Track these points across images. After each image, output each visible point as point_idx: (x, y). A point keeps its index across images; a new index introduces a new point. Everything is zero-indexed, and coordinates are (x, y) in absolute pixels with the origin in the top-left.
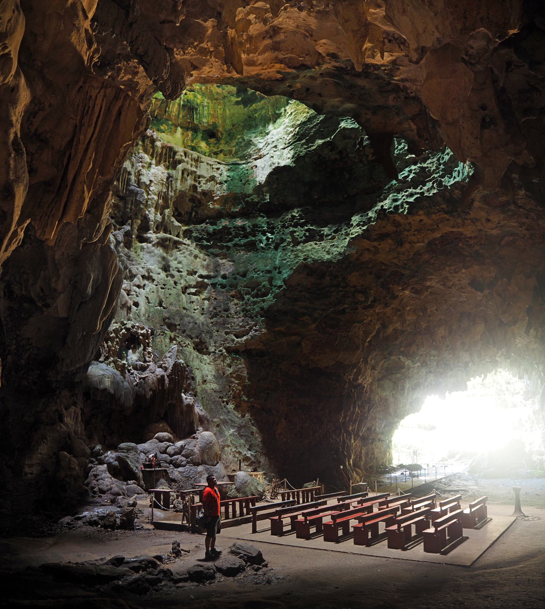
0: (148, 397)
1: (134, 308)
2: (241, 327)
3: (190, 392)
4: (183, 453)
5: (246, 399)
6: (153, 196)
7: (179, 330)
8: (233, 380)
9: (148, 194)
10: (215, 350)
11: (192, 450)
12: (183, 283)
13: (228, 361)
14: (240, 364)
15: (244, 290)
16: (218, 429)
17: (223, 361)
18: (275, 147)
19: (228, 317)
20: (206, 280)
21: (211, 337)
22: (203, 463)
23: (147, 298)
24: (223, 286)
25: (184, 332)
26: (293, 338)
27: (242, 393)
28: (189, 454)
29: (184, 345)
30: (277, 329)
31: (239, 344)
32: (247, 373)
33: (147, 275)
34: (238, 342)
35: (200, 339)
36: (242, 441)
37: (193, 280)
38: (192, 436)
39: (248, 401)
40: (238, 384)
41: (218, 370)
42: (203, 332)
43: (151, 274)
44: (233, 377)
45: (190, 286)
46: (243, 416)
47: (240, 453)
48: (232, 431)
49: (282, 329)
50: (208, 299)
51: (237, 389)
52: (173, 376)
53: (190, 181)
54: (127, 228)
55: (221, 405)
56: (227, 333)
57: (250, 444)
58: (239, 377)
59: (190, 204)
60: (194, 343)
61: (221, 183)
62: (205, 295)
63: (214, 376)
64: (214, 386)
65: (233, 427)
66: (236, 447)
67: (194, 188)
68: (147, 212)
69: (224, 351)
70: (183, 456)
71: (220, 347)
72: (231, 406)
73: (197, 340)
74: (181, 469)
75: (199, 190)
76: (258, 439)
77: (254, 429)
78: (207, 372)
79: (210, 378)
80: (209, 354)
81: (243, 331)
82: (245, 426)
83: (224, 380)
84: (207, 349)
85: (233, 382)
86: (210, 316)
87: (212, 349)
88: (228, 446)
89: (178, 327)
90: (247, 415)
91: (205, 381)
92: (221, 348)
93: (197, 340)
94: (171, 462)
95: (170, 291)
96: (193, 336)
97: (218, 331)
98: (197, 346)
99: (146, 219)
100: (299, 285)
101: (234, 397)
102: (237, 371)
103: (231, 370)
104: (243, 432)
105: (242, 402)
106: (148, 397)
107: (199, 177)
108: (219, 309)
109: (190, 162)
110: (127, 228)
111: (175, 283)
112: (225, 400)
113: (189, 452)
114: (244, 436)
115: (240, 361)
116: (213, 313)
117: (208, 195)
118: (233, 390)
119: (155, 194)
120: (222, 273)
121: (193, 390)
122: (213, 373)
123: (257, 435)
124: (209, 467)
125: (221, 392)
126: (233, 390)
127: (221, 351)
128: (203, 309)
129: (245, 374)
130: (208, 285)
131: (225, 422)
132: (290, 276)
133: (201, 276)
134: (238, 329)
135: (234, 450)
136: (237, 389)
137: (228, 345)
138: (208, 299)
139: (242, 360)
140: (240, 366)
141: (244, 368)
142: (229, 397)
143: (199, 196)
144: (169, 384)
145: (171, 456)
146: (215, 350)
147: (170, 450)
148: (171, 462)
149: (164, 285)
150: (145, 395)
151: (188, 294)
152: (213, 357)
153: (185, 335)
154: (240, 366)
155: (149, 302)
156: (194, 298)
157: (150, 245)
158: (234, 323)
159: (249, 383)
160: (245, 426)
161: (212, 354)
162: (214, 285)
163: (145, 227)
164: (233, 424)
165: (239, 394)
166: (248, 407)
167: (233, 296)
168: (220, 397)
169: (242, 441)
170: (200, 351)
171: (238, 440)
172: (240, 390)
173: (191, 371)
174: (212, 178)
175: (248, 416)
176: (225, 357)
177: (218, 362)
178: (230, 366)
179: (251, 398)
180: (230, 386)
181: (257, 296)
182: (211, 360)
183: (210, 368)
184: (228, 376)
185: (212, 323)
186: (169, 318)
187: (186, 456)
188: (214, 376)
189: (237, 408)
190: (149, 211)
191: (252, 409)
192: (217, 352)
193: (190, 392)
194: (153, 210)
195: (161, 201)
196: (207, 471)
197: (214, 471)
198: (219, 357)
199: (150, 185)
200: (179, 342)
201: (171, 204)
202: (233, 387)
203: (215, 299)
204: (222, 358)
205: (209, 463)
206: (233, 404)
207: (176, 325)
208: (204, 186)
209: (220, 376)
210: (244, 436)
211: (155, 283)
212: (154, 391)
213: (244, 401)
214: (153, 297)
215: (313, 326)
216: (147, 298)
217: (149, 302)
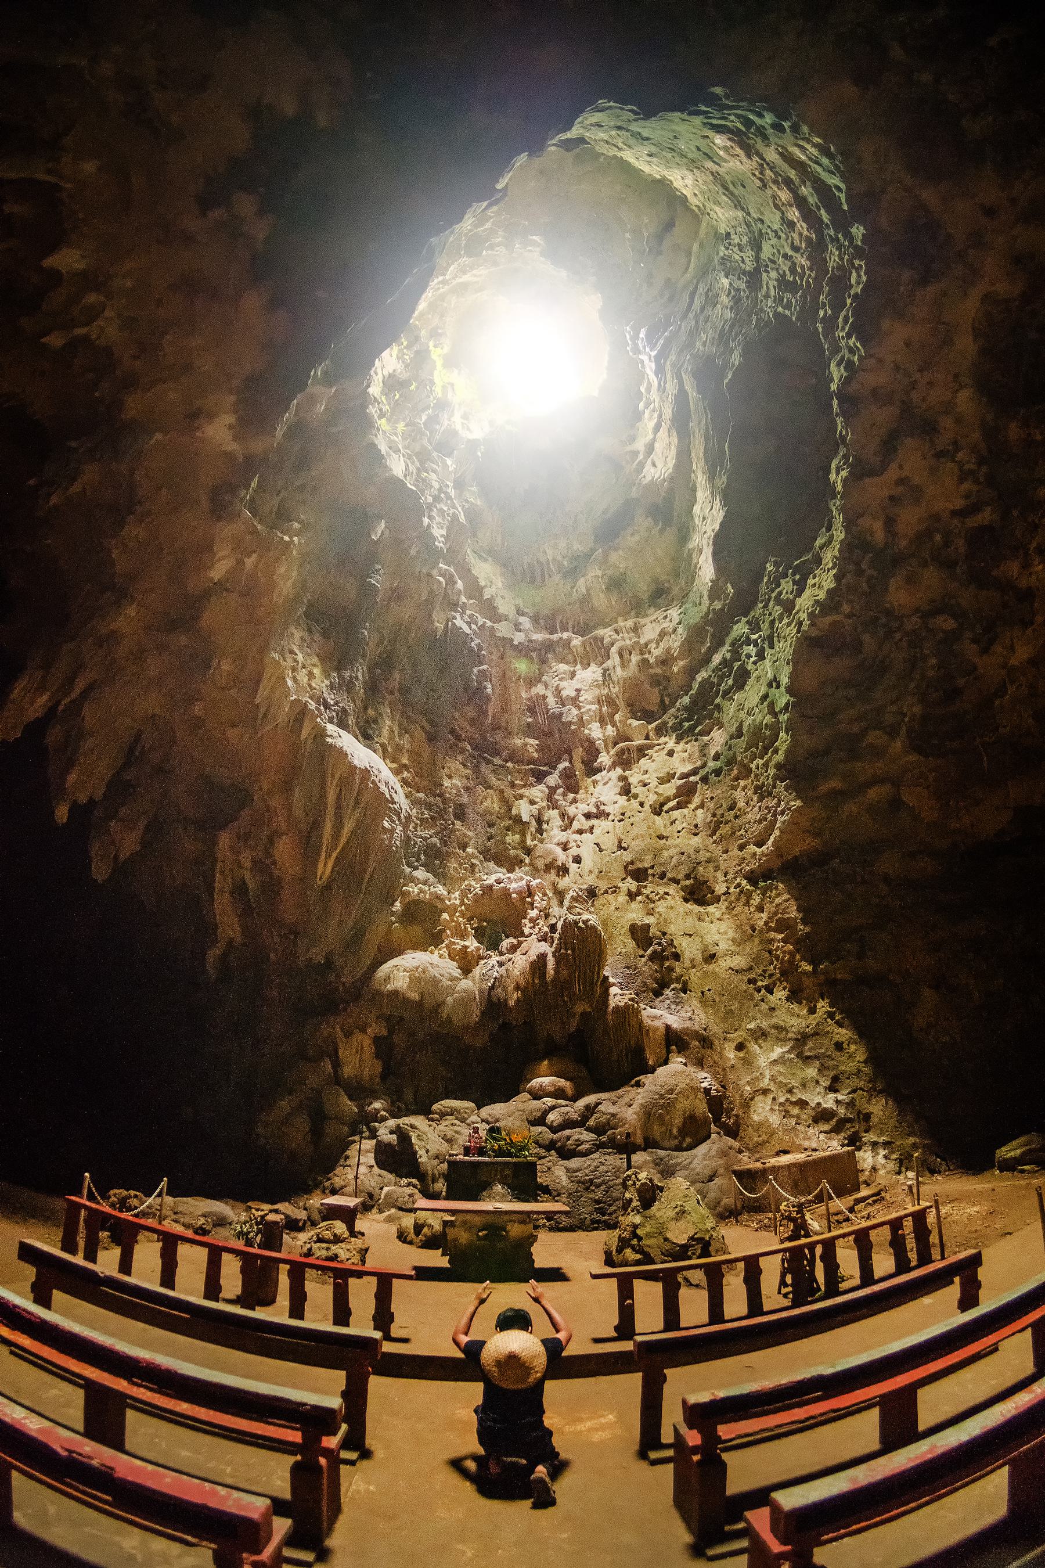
0: (511, 1003)
1: (573, 867)
2: (760, 821)
3: (672, 986)
4: (591, 1122)
5: (809, 968)
6: (588, 707)
7: (654, 875)
8: (772, 935)
9: (580, 708)
10: (728, 888)
11: (614, 1115)
12: (652, 798)
13: (756, 900)
14: (778, 895)
15: (746, 757)
16: (741, 1054)
17: (747, 904)
18: (704, 518)
19: (736, 817)
20: (692, 779)
21: (717, 869)
22: (649, 1144)
23: (597, 844)
24: (717, 772)
25: (663, 876)
26: (873, 793)
27: (798, 957)
28: (604, 1126)
29: (657, 898)
30: (823, 788)
31: (766, 856)
32: (799, 910)
33: (594, 810)
34: (763, 854)
35: (695, 878)
36: (811, 1072)
37: (669, 789)
38: (633, 1082)
39: (815, 971)
40: (784, 940)
41: (740, 927)
42: (699, 863)
43: (602, 807)
44: (770, 929)
45: (669, 799)
46: (812, 1011)
47: (802, 1104)
48: (778, 1051)
49: (835, 783)
50: (702, 806)
51: (784, 952)
52: (563, 951)
53: (635, 659)
54: (564, 765)
55: (752, 999)
56: (741, 848)
57: (832, 1074)
58: (783, 925)
59: (656, 690)
60: (683, 889)
61: (675, 630)
62: (696, 800)
63: (734, 940)
64: (739, 961)
65: (780, 1041)
66: (790, 1091)
67: (645, 661)
68: (586, 731)
69: (744, 882)
70: (589, 1129)
71: (735, 878)
72: (780, 994)
73: (688, 882)
74: (574, 1163)
75: (652, 660)
76: (855, 1057)
77: (843, 1034)
78: (717, 937)
79: (724, 946)
80: (718, 899)
81: (766, 827)
82: (816, 1034)
83: (757, 941)
84: (713, 892)
85: (771, 941)
86: (709, 832)
87: (720, 888)
88: (765, 1092)
89: (650, 871)
90: (819, 1005)
91: (713, 956)
92: (738, 880)
93: (688, 882)
94: (550, 1146)
95: (632, 820)
96: (680, 876)
97: (726, 852)
98: (691, 893)
99: (591, 742)
100: (824, 683)
101: (784, 973)
102: (776, 913)
103: (764, 916)
104: (810, 1049)
105: (804, 978)
106: (511, 1003)
107: (646, 645)
108: (719, 812)
109: (626, 635)
110: (564, 765)
111: (642, 804)
112: (760, 983)
113: (603, 1119)
114: (817, 1057)
115: (776, 888)
116: (713, 825)
117: (665, 661)
118: (777, 959)
119: (593, 703)
120: (713, 753)
121: (678, 980)
122: (731, 934)
123: (853, 1047)
124: (661, 1153)
125: (751, 968)
126: (777, 958)
127: (739, 885)
128: (696, 826)
129: (793, 913)
130: (697, 783)
131: (760, 1035)
132: (793, 676)
133: (684, 776)
134: (757, 829)
135: (782, 1100)
136: (784, 952)
137: (748, 868)
138: (702, 806)
139: (781, 886)
140: (778, 900)
141: (787, 901)
142: (771, 976)
143: (658, 671)
144: (555, 970)
145: (554, 1130)
146: (728, 888)
147: (552, 1117)
148: (550, 1146)
149: (623, 814)
150: (505, 1000)
151: (666, 812)
152: (726, 904)
153: (665, 880)
154: (778, 900)
155: (601, 850)
156: (676, 814)
157: (604, 773)
158: (749, 823)
159: (807, 929)
160: (816, 1034)
161: (723, 898)
162: (705, 780)
163: (592, 752)
164: (782, 1036)
165: (792, 962)
166: (820, 984)
167: (737, 779)
168: (750, 981)
169: (811, 1072)
170: (701, 902)
171: (798, 1072)
172: (790, 952)
173: (671, 943)
174: (663, 634)
175: (823, 1006)
176: (749, 897)
177: (738, 909)
178: (760, 909)
179: (821, 963)
180: (770, 952)
181: (766, 750)
182: (724, 910)
183: (723, 926)
184: (761, 931)
185: (715, 842)
186: (632, 863)
187: (599, 1130)
188: (734, 940)
189: (794, 996)
190: (590, 729)
191: (830, 988)
192: (732, 890)
193: (672, 986)
194: (595, 725)
195: (605, 709)
196: (657, 1165)
197: (677, 1164)
198: (738, 899)
199: (578, 696)
200: (647, 896)
201: (621, 704)
202: (776, 950)
203: (712, 798)
204: (743, 899)
205: (666, 1144)
206: (784, 989)
207: (646, 870)
208: (657, 652)
209: (748, 933)
210: (817, 1057)
211: (611, 817)
212: (524, 991)
213: (805, 973)
214: (609, 843)
215: (897, 745)
216: (597, 844)
217: (601, 850)
